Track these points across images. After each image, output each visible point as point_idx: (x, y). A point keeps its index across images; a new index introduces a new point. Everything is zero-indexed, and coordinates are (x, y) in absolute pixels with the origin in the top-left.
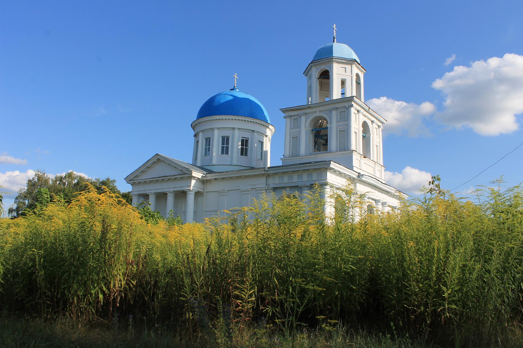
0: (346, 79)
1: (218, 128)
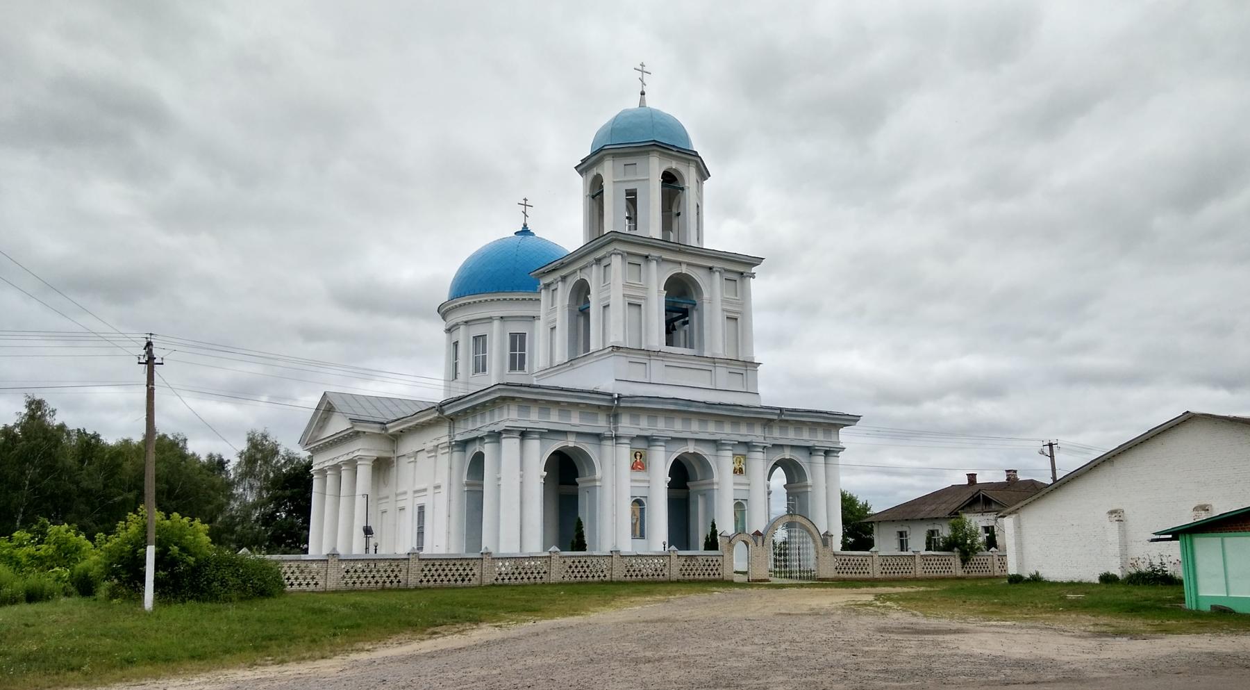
0: (636, 189)
1: (466, 322)
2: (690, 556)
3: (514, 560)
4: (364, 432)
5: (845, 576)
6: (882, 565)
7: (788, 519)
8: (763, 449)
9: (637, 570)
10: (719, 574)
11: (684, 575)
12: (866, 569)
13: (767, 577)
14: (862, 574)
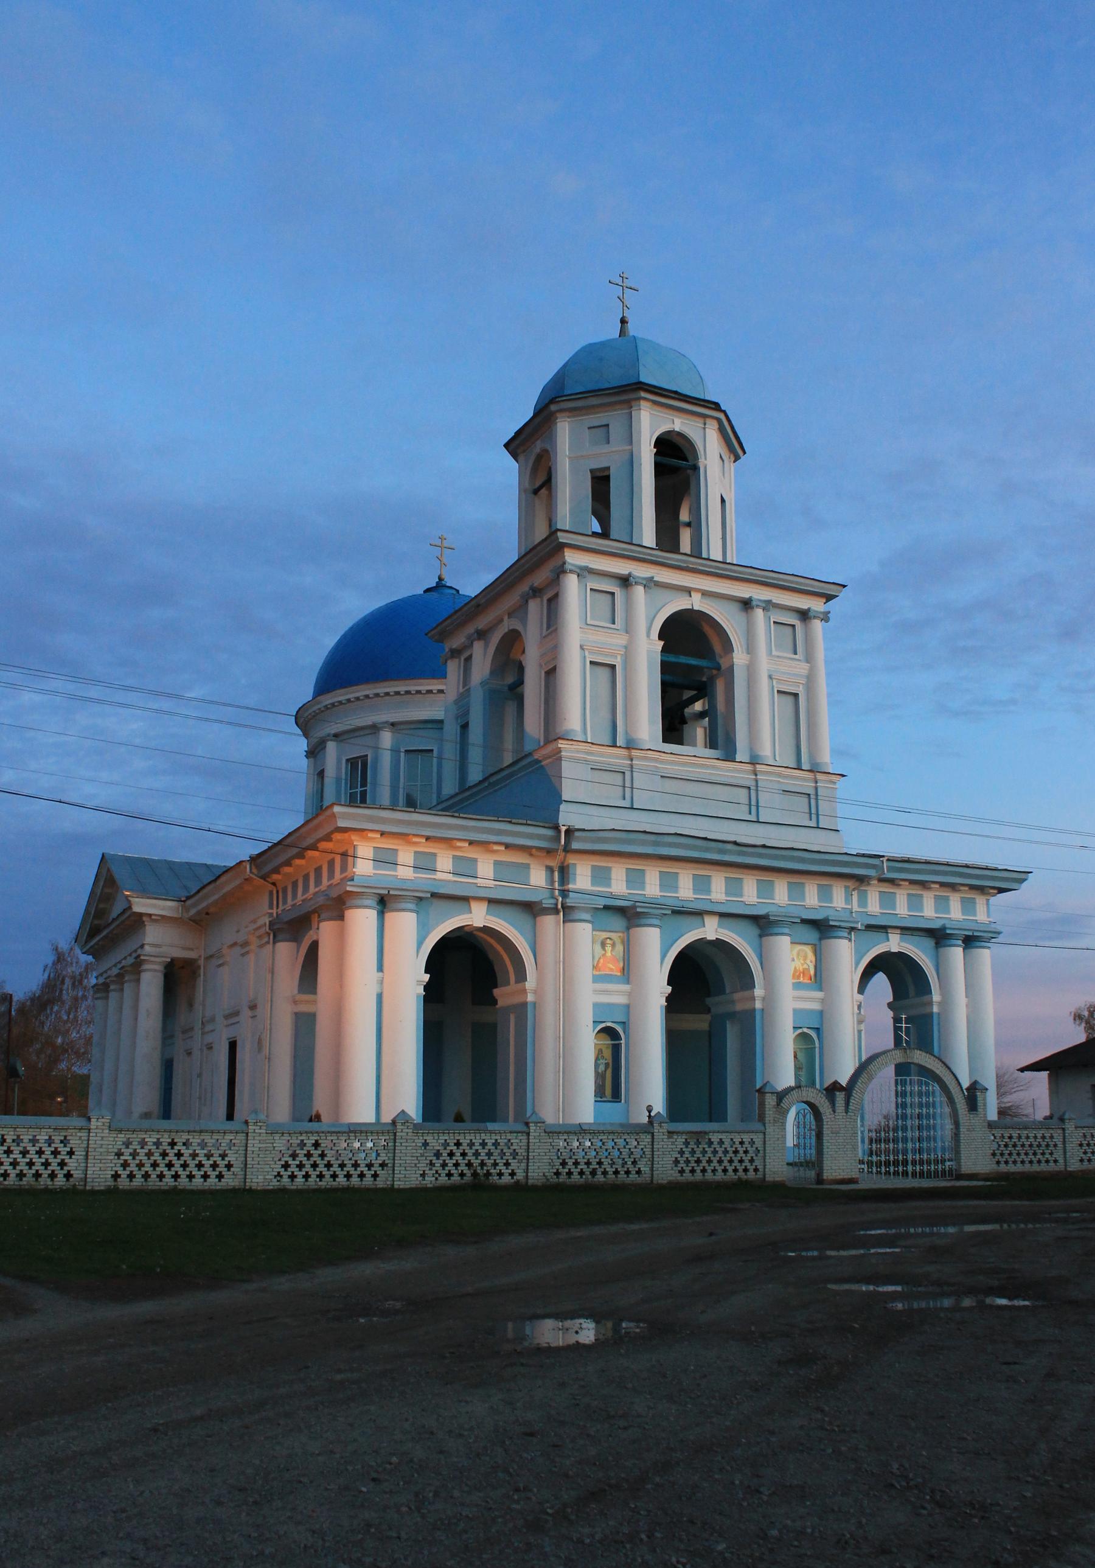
2: (696, 1133)
3: (515, 1134)
4: (150, 915)
5: (1011, 1168)
6: (1081, 1145)
7: (899, 1057)
8: (850, 933)
9: (582, 1161)
10: (756, 1170)
11: (682, 1172)
12: (1051, 1154)
13: (854, 1174)
14: (1043, 1164)
